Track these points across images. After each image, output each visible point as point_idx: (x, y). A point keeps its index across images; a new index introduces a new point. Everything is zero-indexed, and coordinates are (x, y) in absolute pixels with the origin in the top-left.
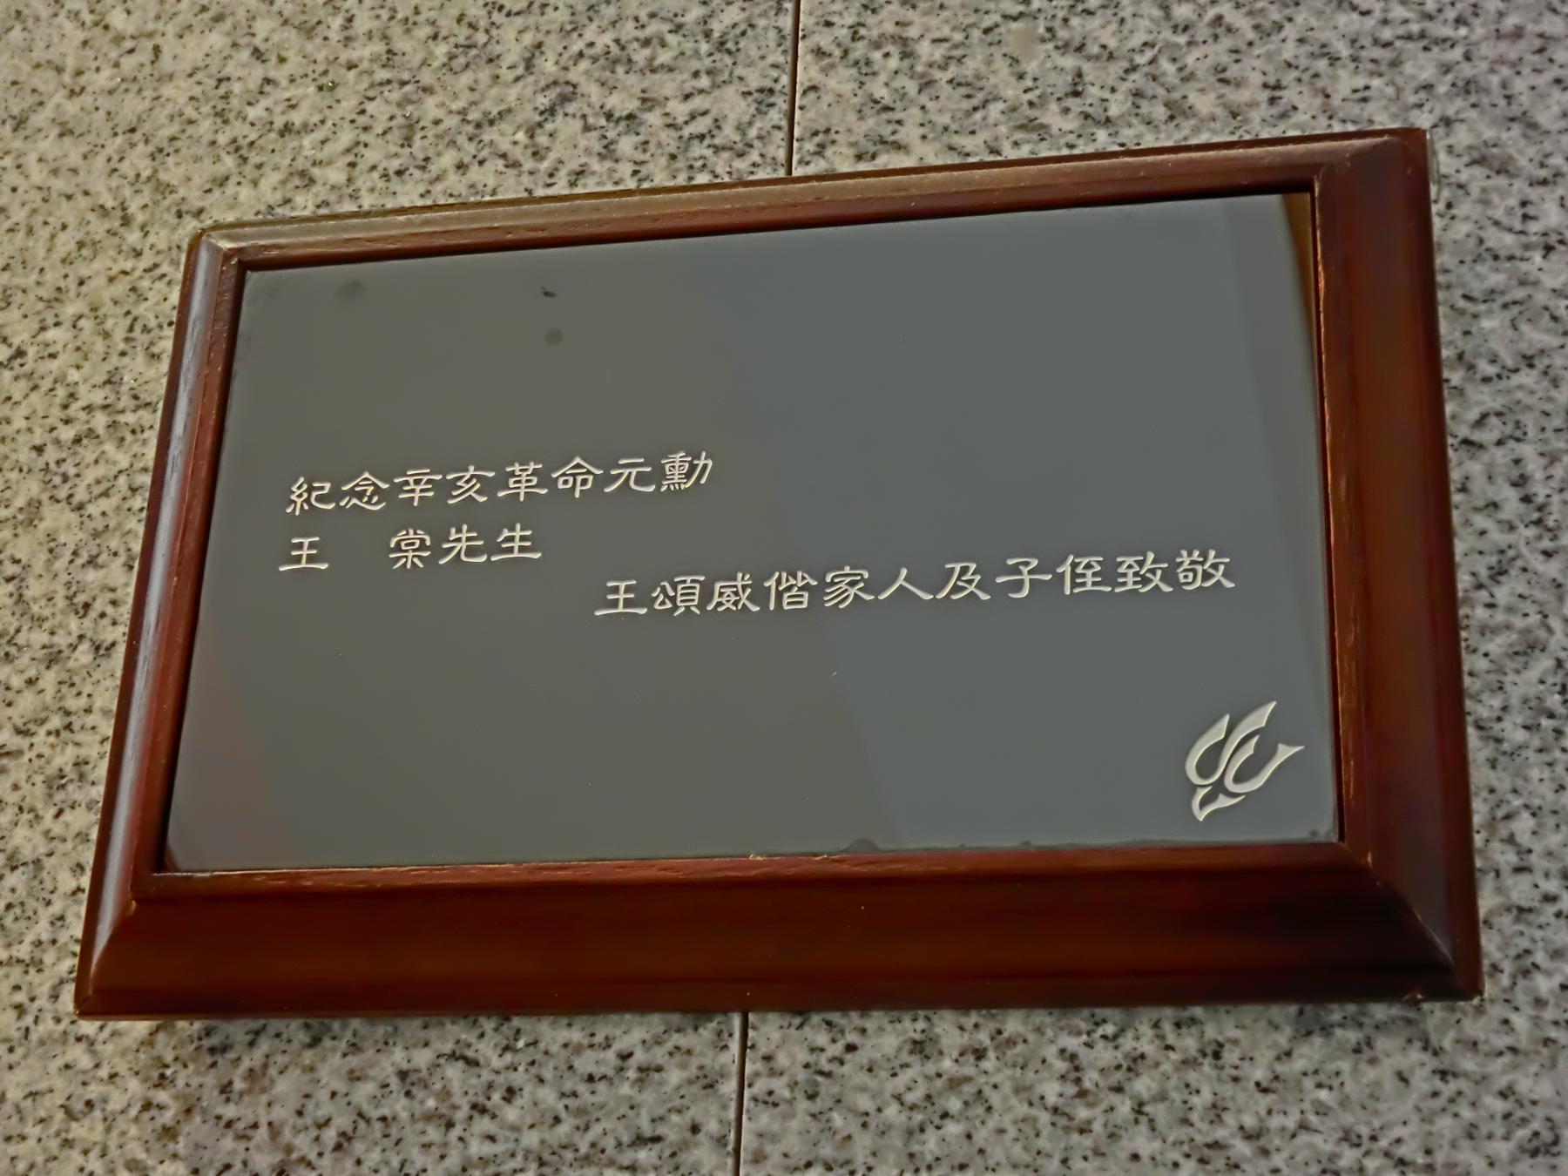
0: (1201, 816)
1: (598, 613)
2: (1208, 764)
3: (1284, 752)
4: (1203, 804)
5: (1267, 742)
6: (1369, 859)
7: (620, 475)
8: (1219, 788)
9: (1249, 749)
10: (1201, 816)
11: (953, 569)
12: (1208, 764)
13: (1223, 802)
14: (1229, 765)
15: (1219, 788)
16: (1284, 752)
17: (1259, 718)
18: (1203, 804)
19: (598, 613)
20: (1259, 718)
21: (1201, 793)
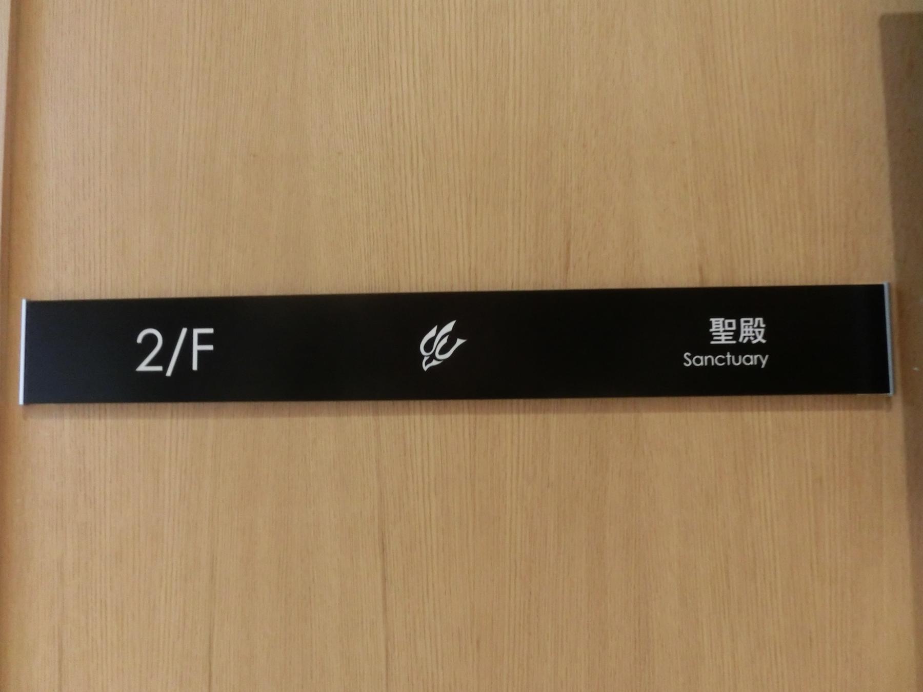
0: (425, 368)
1: (195, 367)
2: (429, 346)
3: (460, 342)
4: (427, 363)
5: (452, 337)
6: (916, 369)
7: (150, 364)
8: (433, 357)
9: (445, 341)
10: (425, 368)
11: (150, 364)
12: (429, 346)
13: (434, 363)
14: (438, 346)
15: (433, 357)
16: (460, 342)
17: (449, 327)
18: (427, 363)
19: (195, 367)
20: (449, 327)
21: (426, 359)
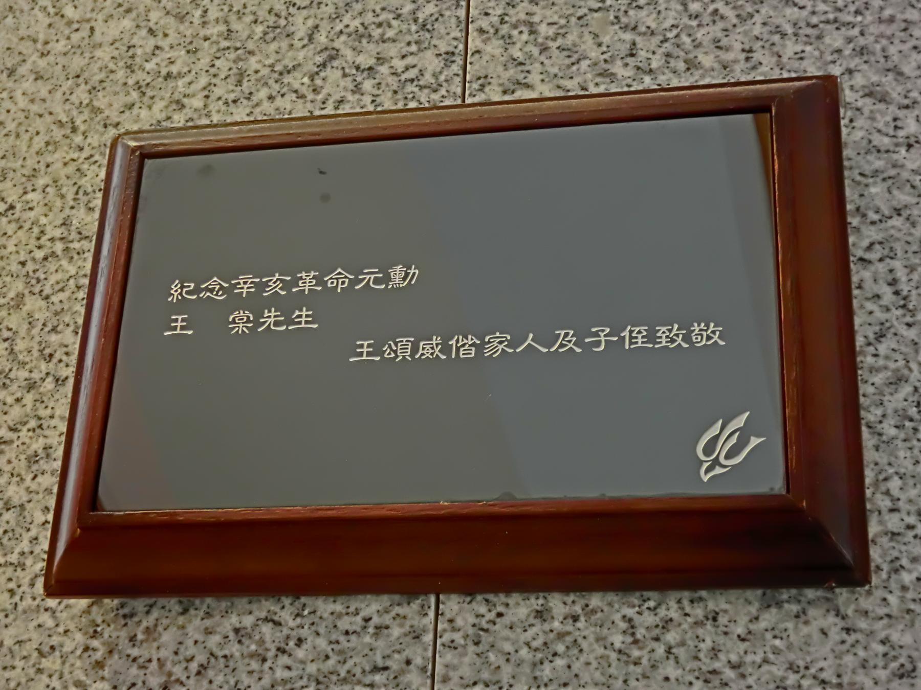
0: (706, 479)
1: (351, 360)
2: (710, 448)
3: (754, 441)
4: (707, 472)
5: (744, 435)
6: (804, 504)
7: (364, 279)
8: (716, 462)
9: (734, 440)
10: (706, 479)
11: (560, 334)
12: (710, 448)
13: (718, 471)
14: (722, 449)
15: (716, 462)
16: (754, 441)
17: (740, 422)
18: (707, 472)
19: (351, 360)
20: (740, 422)
21: (706, 465)
